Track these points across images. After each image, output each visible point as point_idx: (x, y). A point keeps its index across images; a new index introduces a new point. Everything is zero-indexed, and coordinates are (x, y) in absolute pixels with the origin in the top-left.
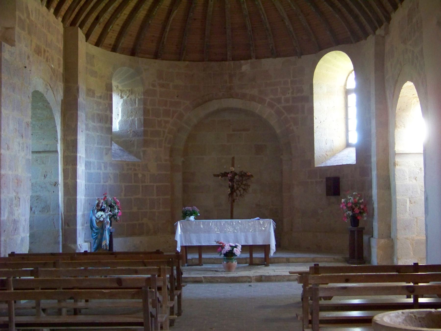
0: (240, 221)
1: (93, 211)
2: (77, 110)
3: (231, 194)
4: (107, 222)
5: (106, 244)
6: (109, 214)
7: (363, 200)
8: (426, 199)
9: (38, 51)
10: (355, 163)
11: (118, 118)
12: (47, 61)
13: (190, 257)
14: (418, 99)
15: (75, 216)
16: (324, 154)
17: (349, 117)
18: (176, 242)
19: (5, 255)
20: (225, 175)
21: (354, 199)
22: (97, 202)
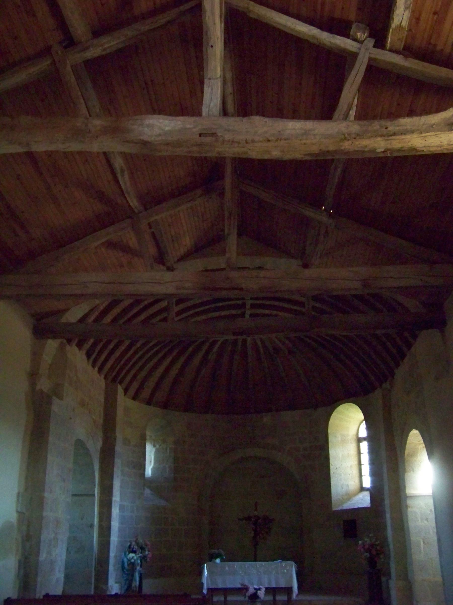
0: (263, 563)
1: (125, 554)
2: (114, 457)
3: (255, 537)
4: (138, 564)
5: (135, 586)
6: (140, 556)
7: (379, 542)
8: (439, 540)
9: (83, 404)
10: (370, 506)
11: (150, 465)
12: (89, 412)
13: (215, 599)
14: (424, 445)
15: (108, 557)
16: (341, 498)
17: (362, 462)
18: (202, 584)
19: (39, 597)
20: (248, 518)
21: (370, 540)
22: (129, 544)
